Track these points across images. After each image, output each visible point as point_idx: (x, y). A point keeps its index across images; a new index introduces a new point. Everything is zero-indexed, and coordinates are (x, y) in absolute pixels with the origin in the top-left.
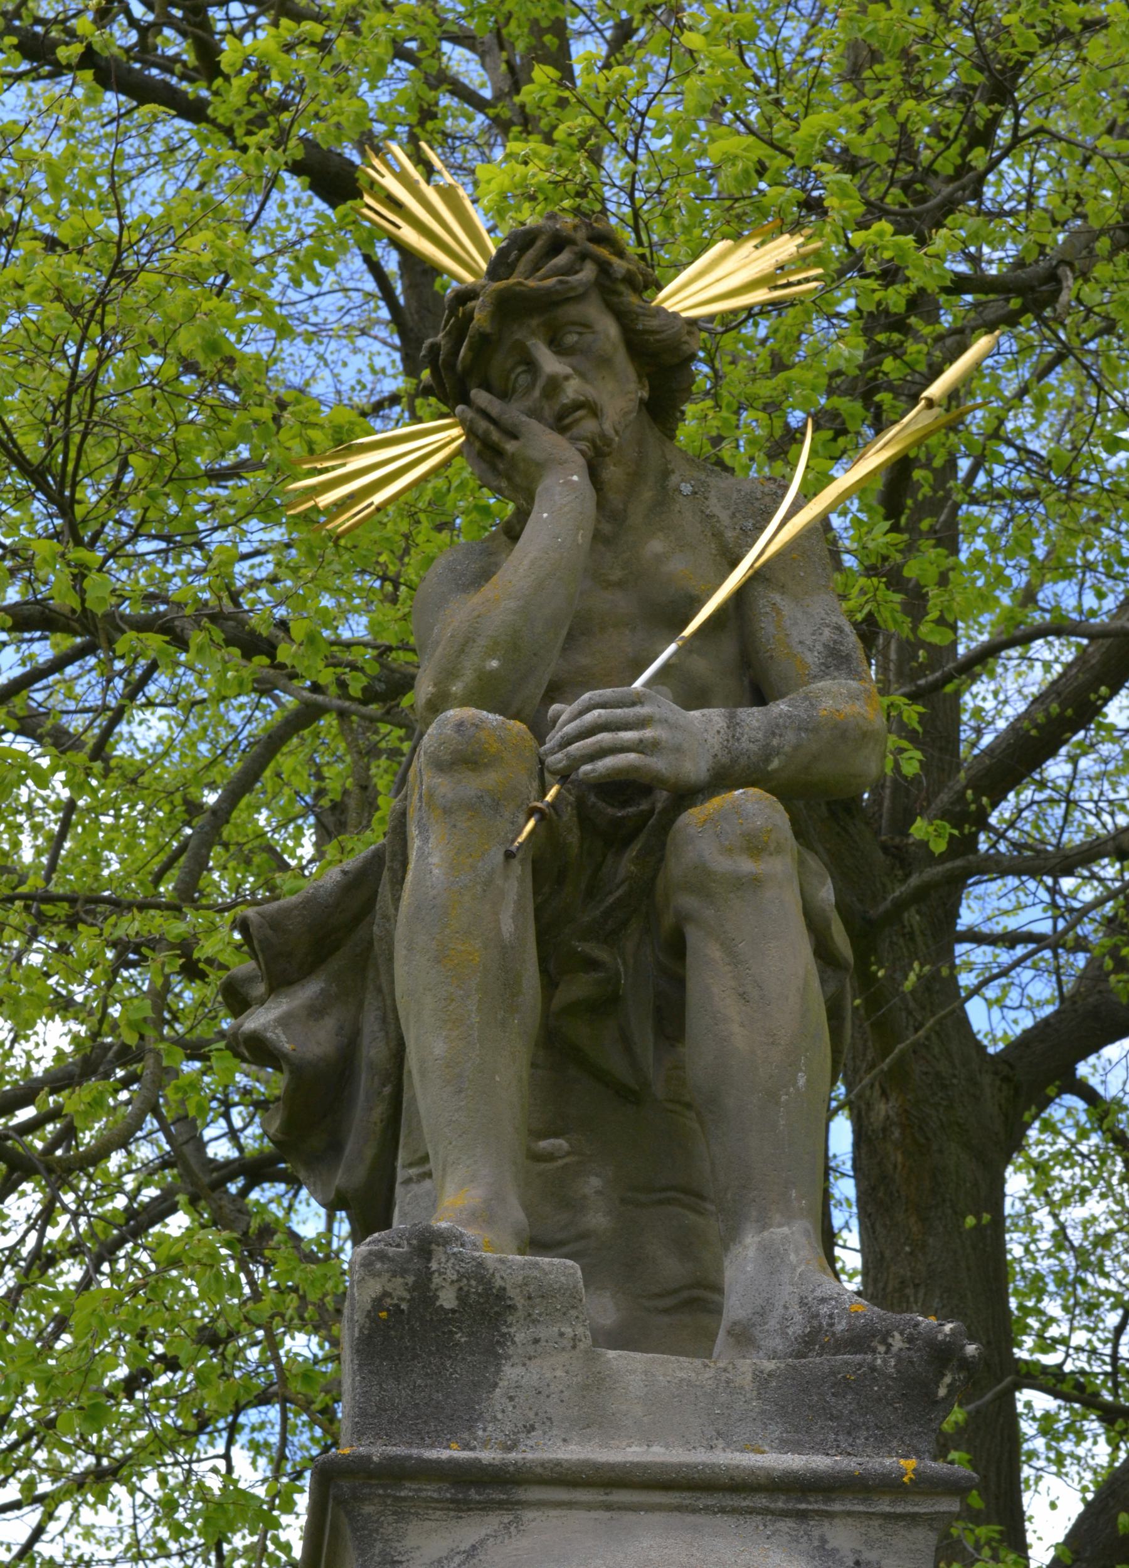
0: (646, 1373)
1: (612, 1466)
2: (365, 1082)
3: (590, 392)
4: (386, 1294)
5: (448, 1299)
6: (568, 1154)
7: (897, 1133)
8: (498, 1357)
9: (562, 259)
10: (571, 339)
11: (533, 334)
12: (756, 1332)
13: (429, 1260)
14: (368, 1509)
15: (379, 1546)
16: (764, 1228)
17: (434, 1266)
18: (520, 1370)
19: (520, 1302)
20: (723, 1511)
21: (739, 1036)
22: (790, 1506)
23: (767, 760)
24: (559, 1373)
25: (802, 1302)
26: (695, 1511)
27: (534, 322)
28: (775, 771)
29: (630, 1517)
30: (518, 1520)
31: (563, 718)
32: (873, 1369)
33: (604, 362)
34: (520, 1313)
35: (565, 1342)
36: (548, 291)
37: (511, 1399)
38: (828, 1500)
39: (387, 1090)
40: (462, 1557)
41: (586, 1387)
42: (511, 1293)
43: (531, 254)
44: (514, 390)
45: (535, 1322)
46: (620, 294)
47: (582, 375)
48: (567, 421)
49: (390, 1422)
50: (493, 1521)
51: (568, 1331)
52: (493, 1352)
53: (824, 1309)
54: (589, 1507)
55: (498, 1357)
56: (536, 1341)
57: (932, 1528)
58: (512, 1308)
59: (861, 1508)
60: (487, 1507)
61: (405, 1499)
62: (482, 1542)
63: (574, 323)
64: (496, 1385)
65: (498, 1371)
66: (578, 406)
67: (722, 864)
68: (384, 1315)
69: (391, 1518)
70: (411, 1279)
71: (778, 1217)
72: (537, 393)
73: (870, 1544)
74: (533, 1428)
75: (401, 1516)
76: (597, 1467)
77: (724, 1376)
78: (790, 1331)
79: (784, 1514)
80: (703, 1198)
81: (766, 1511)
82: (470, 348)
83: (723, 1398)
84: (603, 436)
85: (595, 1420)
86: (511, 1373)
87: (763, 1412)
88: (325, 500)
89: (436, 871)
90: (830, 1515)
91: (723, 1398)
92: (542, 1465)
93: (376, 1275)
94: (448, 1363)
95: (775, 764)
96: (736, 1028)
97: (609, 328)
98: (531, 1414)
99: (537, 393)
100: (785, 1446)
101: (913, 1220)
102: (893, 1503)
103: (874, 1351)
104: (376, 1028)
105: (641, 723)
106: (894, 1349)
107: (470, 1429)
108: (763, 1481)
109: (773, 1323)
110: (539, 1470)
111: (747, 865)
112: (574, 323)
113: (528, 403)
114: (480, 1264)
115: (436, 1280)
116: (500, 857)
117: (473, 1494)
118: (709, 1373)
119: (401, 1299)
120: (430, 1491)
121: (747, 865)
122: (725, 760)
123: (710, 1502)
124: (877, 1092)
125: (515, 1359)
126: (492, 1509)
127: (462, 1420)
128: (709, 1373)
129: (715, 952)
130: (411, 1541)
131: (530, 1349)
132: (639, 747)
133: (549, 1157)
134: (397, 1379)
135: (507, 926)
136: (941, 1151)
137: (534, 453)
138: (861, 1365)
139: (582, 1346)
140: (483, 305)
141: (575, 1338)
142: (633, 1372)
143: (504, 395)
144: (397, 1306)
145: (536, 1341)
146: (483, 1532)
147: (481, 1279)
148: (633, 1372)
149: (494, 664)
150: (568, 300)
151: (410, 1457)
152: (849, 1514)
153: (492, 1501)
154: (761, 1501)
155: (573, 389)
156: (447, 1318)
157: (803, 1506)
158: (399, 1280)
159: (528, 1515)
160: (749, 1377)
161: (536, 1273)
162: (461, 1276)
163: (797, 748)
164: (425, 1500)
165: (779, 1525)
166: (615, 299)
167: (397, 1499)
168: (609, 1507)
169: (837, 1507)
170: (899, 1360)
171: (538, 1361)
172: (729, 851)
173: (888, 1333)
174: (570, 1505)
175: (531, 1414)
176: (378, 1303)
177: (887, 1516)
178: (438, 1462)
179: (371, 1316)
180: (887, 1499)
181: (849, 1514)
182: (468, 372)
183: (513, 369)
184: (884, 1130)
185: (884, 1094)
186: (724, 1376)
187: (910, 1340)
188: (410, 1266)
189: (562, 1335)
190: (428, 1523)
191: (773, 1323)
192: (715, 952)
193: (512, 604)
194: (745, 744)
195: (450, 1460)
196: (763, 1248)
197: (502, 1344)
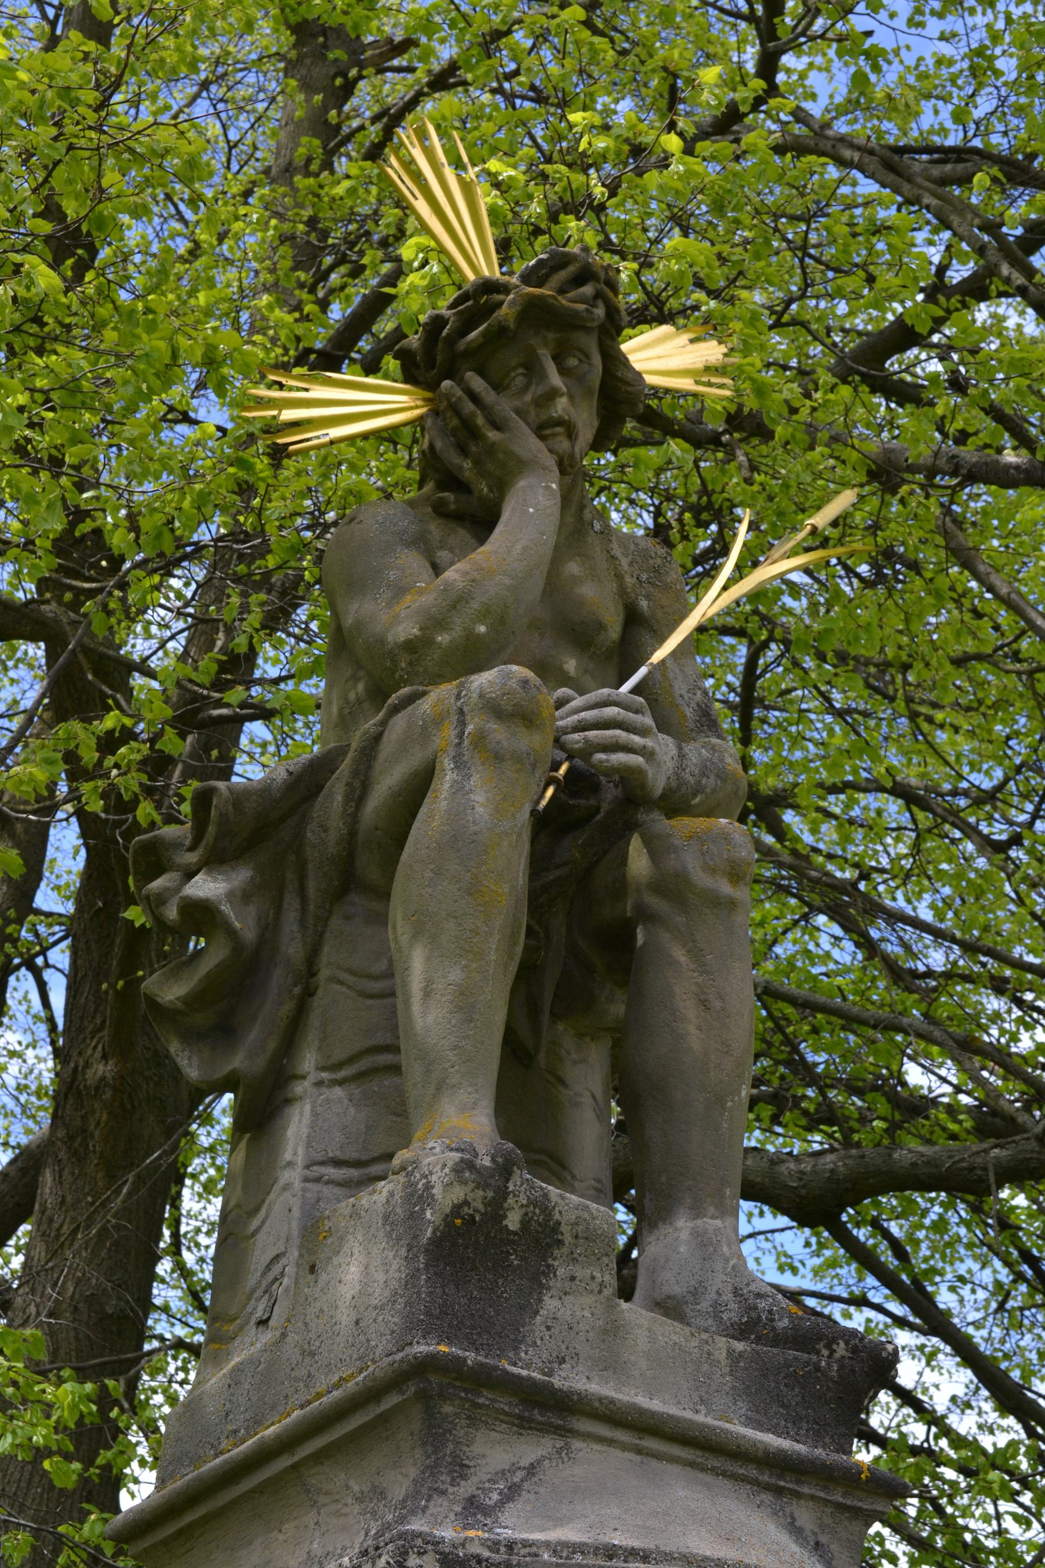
0: (649, 1330)
1: (653, 1414)
2: (278, 978)
4: (466, 1203)
5: (513, 1221)
7: (108, 1095)
9: (588, 290)
10: (572, 362)
11: (546, 345)
12: (688, 1310)
13: (507, 1180)
14: (447, 1409)
15: (451, 1446)
16: (698, 1215)
18: (556, 1302)
19: (568, 1238)
20: (724, 1474)
21: (694, 1037)
22: (773, 1481)
24: (587, 1314)
25: (736, 1292)
26: (704, 1469)
27: (551, 336)
29: (654, 1463)
31: (573, 704)
32: (818, 1368)
34: (565, 1250)
35: (595, 1287)
36: (576, 314)
38: (798, 1482)
39: (297, 990)
40: (524, 1473)
41: (605, 1332)
42: (564, 1228)
43: (563, 275)
44: (506, 388)
45: (575, 1260)
47: (571, 397)
48: (547, 432)
49: (450, 1326)
52: (537, 1279)
53: (762, 1304)
54: (624, 1447)
55: (541, 1286)
56: (573, 1279)
58: (560, 1243)
59: (822, 1495)
60: (545, 1429)
62: (539, 1461)
64: (537, 1313)
65: (540, 1300)
66: (560, 422)
67: (702, 879)
68: (458, 1221)
69: (464, 1422)
70: (490, 1194)
71: (712, 1210)
72: (528, 398)
75: (473, 1422)
76: (643, 1412)
77: (706, 1348)
78: (725, 1316)
79: (767, 1488)
80: (563, 1166)
82: (484, 334)
83: (705, 1367)
85: (611, 1365)
86: (550, 1303)
87: (734, 1388)
88: (289, 415)
89: (480, 809)
90: (798, 1495)
92: (600, 1400)
93: (463, 1182)
94: (500, 1282)
96: (692, 1029)
99: (528, 398)
100: (749, 1422)
101: (100, 1175)
102: (844, 1495)
103: (818, 1353)
104: (295, 928)
106: (837, 1355)
107: (516, 1349)
108: (760, 1454)
109: (705, 1305)
110: (597, 1404)
111: (726, 888)
112: (581, 351)
113: (517, 403)
115: (511, 1201)
119: (476, 1210)
120: (503, 1403)
121: (726, 888)
122: (674, 784)
123: (717, 1464)
124: (98, 1054)
126: (548, 1432)
129: (680, 955)
130: (477, 1449)
131: (567, 1284)
134: (457, 1286)
136: (141, 1120)
137: (522, 452)
138: (808, 1363)
139: (607, 1292)
140: (513, 302)
141: (602, 1284)
142: (640, 1327)
143: (498, 387)
144: (472, 1217)
145: (573, 1279)
146: (540, 1452)
148: (640, 1327)
149: (482, 629)
151: (497, 1368)
152: (813, 1498)
153: (551, 1425)
154: (752, 1472)
156: (508, 1239)
158: (480, 1193)
159: (577, 1444)
161: (586, 1215)
164: (498, 1411)
165: (763, 1496)
166: (609, 342)
167: (476, 1405)
168: (639, 1451)
169: (805, 1490)
170: (842, 1367)
172: (713, 871)
173: (834, 1340)
174: (610, 1442)
176: (457, 1209)
178: (519, 1377)
179: (448, 1220)
181: (813, 1498)
182: (469, 353)
183: (514, 369)
184: (97, 1088)
185: (105, 1057)
186: (706, 1348)
187: (855, 1350)
188: (492, 1182)
189: (593, 1278)
190: (493, 1434)
191: (705, 1305)
192: (680, 955)
193: (507, 581)
195: (529, 1378)
196: (696, 1234)
197: (546, 1275)
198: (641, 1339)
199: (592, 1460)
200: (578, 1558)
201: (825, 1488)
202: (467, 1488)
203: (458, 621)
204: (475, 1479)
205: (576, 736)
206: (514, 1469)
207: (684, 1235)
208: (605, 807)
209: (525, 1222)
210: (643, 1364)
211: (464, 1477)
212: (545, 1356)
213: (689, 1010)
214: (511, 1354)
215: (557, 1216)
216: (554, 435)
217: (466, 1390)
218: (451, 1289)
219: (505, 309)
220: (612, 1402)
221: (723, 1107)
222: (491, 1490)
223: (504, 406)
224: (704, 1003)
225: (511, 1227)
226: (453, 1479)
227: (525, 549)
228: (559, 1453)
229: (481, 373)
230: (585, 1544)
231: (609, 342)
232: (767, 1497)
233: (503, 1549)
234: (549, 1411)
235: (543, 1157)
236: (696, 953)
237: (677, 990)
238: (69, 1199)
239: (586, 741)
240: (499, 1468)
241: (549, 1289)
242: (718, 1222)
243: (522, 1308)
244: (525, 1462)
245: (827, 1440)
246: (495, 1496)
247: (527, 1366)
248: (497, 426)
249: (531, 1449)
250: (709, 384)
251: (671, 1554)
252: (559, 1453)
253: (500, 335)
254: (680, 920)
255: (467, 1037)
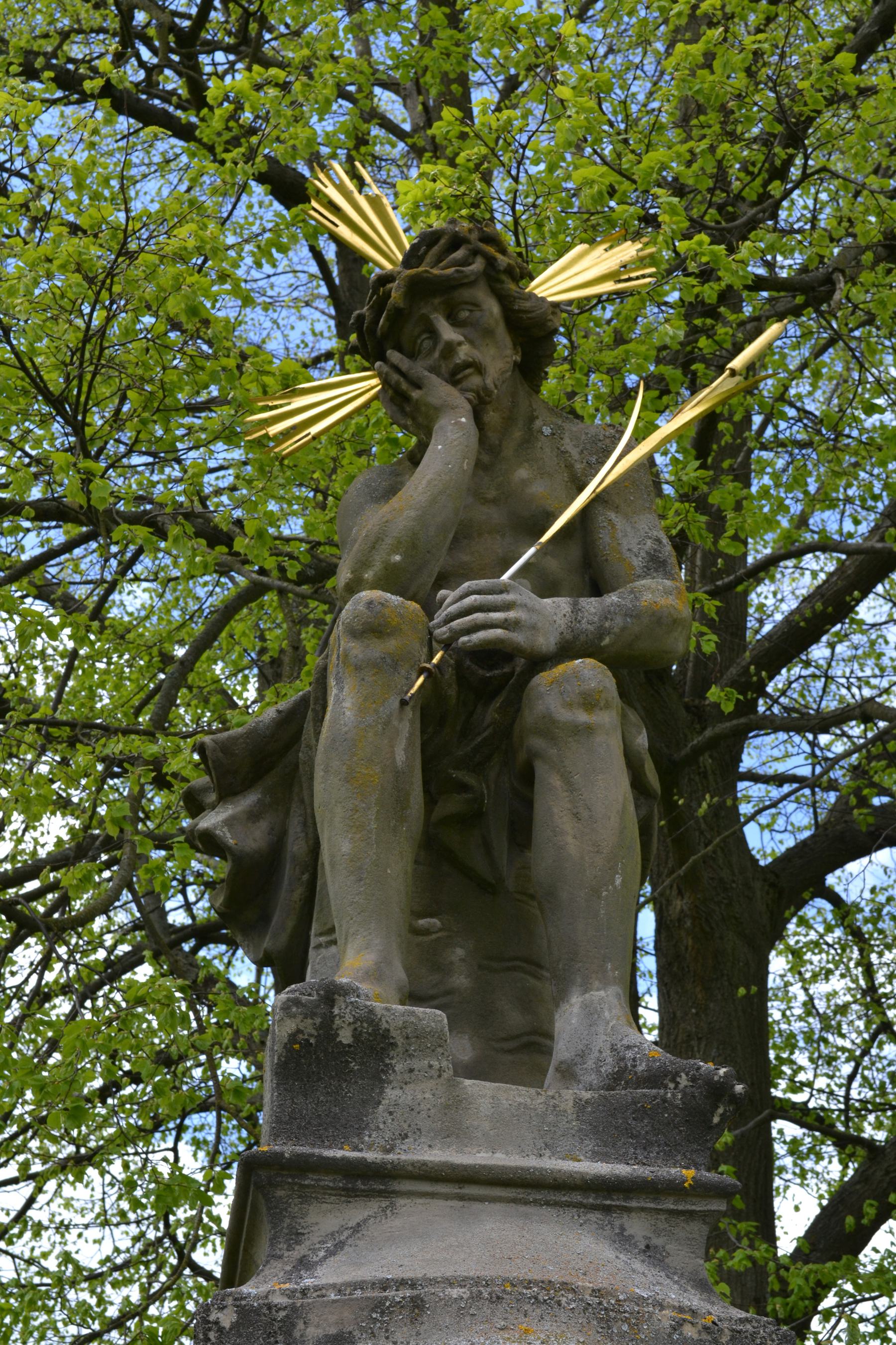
1: (465, 1167)
2: (289, 871)
3: (477, 355)
4: (299, 1031)
5: (345, 1037)
6: (440, 930)
7: (689, 923)
8: (382, 1081)
9: (459, 254)
10: (464, 314)
12: (577, 1070)
13: (332, 1007)
14: (280, 1193)
15: (287, 1221)
16: (586, 991)
17: (336, 1011)
18: (398, 1092)
19: (400, 1041)
20: (547, 1204)
21: (572, 846)
22: (598, 1202)
23: (601, 637)
24: (427, 1095)
25: (613, 1048)
26: (526, 1203)
27: (437, 301)
28: (607, 646)
29: (477, 1206)
30: (392, 1205)
32: (664, 1100)
33: (488, 333)
35: (434, 1073)
36: (448, 278)
37: (391, 1113)
38: (627, 1199)
39: (305, 877)
41: (447, 1107)
42: (394, 1033)
43: (436, 249)
44: (420, 352)
45: (411, 1056)
46: (502, 282)
47: (471, 342)
49: (299, 1128)
50: (374, 1206)
51: (435, 1063)
52: (378, 1078)
53: (629, 1054)
54: (447, 1197)
55: (382, 1081)
56: (411, 1071)
57: (705, 1223)
58: (394, 1045)
59: (652, 1205)
61: (308, 1186)
62: (365, 1221)
63: (467, 303)
64: (379, 1103)
65: (382, 1092)
66: (467, 365)
67: (564, 715)
68: (297, 1046)
70: (318, 1021)
71: (596, 984)
72: (437, 354)
73: (658, 1233)
74: (406, 1136)
77: (552, 1102)
78: (603, 1070)
79: (594, 1208)
80: (540, 966)
81: (579, 1205)
82: (388, 319)
83: (551, 1118)
84: (485, 388)
86: (391, 1094)
87: (580, 1130)
89: (348, 713)
90: (628, 1210)
91: (551, 1118)
93: (292, 1016)
95: (607, 641)
96: (570, 839)
97: (493, 307)
98: (405, 1126)
99: (437, 354)
100: (596, 1156)
101: (698, 989)
102: (676, 1202)
103: (666, 1087)
104: (299, 830)
105: (507, 607)
106: (681, 1086)
107: (359, 1135)
108: (579, 1182)
109: (590, 1064)
110: (410, 1168)
111: (582, 717)
112: (467, 303)
114: (371, 1011)
115: (337, 1021)
116: (396, 704)
117: (360, 1185)
118: (541, 1099)
119: (311, 1035)
120: (327, 1181)
121: (582, 717)
122: (569, 637)
125: (395, 1084)
127: (353, 1127)
128: (541, 1099)
129: (556, 781)
130: (312, 1218)
131: (407, 1077)
132: (504, 625)
133: (426, 932)
134: (305, 1096)
135: (400, 756)
136: (721, 938)
137: (433, 400)
138: (655, 1097)
139: (445, 1075)
140: (399, 287)
141: (440, 1070)
143: (412, 355)
144: (307, 1040)
145: (411, 1071)
147: (371, 1022)
149: (398, 558)
150: (463, 285)
151: (313, 1155)
152: (643, 1209)
153: (374, 1190)
154: (577, 1197)
155: (464, 352)
157: (608, 1202)
158: (310, 1021)
159: (401, 1201)
160: (571, 1103)
161: (413, 1019)
162: (356, 1020)
163: (623, 629)
164: (323, 1187)
166: (498, 286)
167: (302, 1186)
168: (461, 1198)
169: (634, 1204)
171: (412, 1086)
172: (569, 706)
173: (677, 1074)
174: (433, 1195)
175: (405, 1126)
177: (671, 1212)
178: (334, 1159)
180: (672, 1199)
181: (643, 1209)
183: (419, 336)
184: (679, 920)
186: (552, 1102)
187: (693, 1079)
189: (431, 1066)
191: (590, 1064)
192: (556, 781)
193: (413, 514)
194: (584, 625)
195: (343, 1158)
196: (585, 1006)
198: (485, 1106)
199: (412, 1212)
200: (358, 1293)
201: (654, 1200)
202: (300, 1251)
203: (377, 558)
204: (308, 1243)
205: (444, 629)
206: (344, 1228)
207: (576, 1010)
208: (518, 669)
209: (356, 1035)
210: (486, 1125)
211: (299, 1243)
212: (388, 1135)
213: (567, 824)
214: (355, 1140)
215: (384, 1025)
216: (466, 377)
217: (293, 1177)
218: (300, 1100)
219: (393, 294)
220: (425, 1164)
221: (599, 897)
222: (319, 1249)
223: (419, 369)
224: (576, 816)
225: (345, 1042)
226: (289, 1245)
227: (429, 483)
228: (384, 1211)
229: (400, 350)
230: (364, 1282)
231: (498, 286)
232: (594, 1216)
233: (298, 1295)
234: (373, 1182)
235: (518, 963)
236: (567, 779)
237: (555, 810)
238: (679, 1014)
239: (451, 630)
240: (330, 1231)
241: (390, 1082)
242: (602, 993)
243: (364, 1102)
244: (353, 1223)
245: (679, 1158)
246: (322, 1254)
247: (370, 1147)
248: (418, 386)
249: (356, 1212)
250: (630, 279)
251: (435, 1279)
252: (384, 1211)
253: (398, 316)
254: (553, 752)
255: (360, 893)
